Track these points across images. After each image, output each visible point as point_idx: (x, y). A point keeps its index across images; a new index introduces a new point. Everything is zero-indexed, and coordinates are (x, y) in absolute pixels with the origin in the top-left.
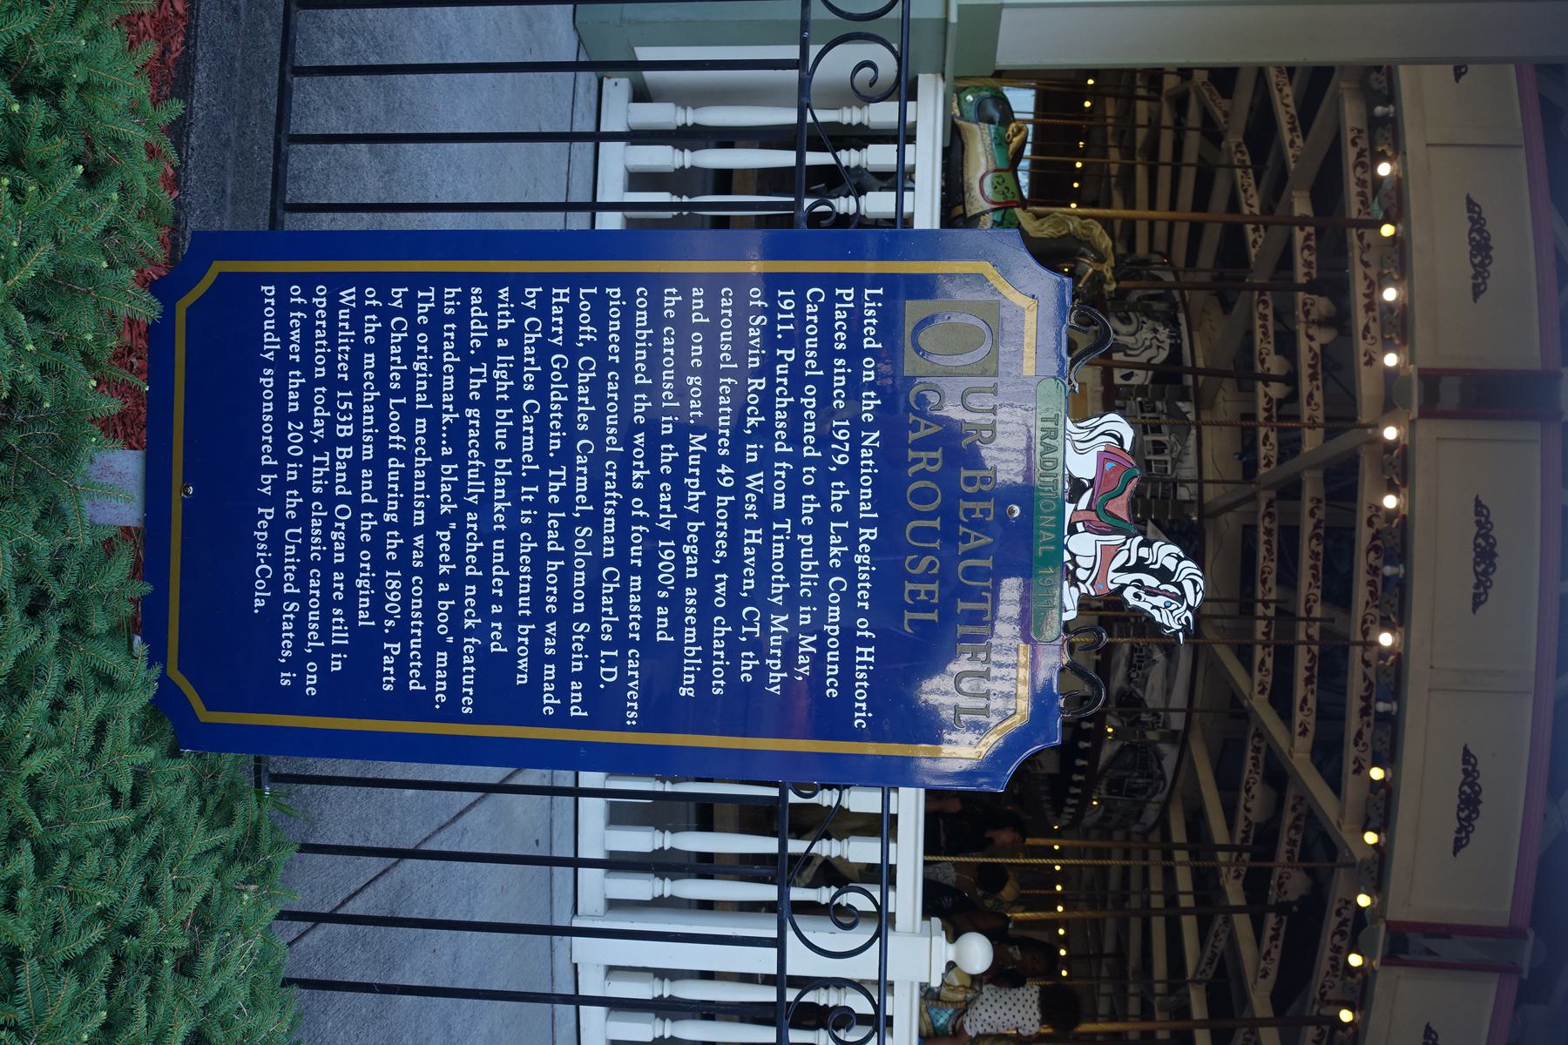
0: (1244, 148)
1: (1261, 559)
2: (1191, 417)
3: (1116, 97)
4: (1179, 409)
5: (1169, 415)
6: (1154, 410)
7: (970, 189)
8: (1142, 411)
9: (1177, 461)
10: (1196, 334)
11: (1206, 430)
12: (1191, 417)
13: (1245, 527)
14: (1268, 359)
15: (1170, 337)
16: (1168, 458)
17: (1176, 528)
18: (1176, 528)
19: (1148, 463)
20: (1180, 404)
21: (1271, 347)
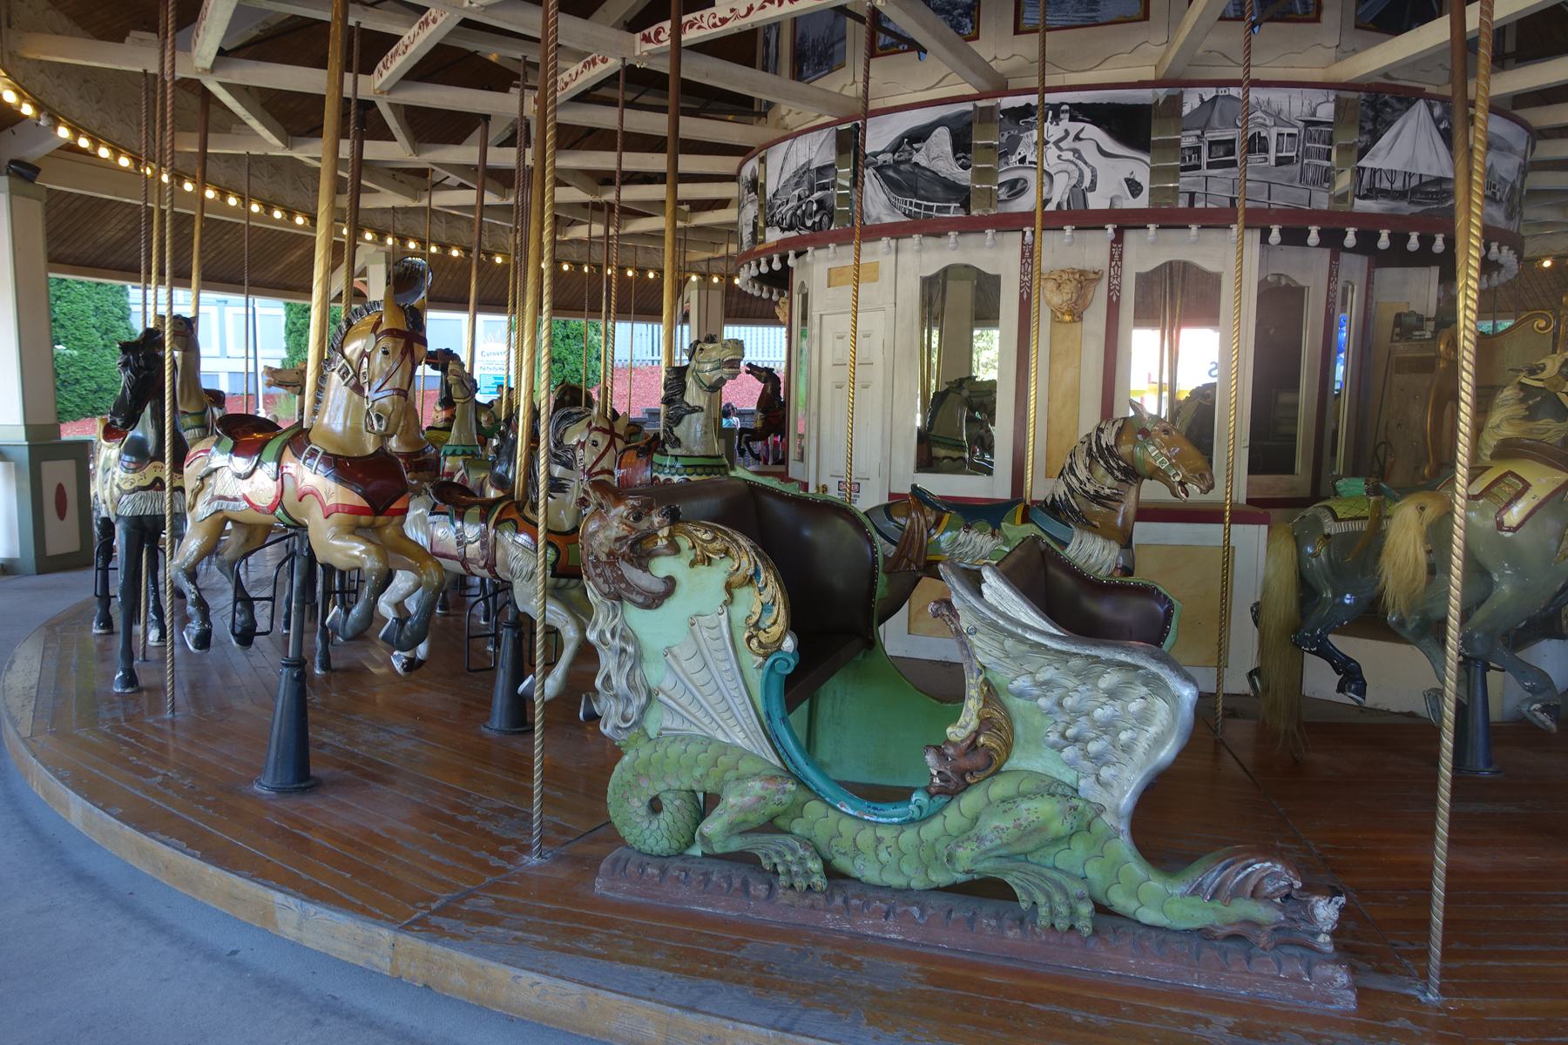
0: (652, 30)
1: (702, 33)
2: (1209, 93)
3: (358, 190)
4: (1194, 113)
5: (1205, 127)
6: (1197, 150)
7: (1096, 645)
8: (1198, 167)
9: (1278, 119)
10: (1013, 85)
11: (1255, 74)
12: (1209, 93)
13: (1357, 27)
14: (720, 15)
15: (1056, 118)
16: (1274, 132)
17: (1369, 126)
18: (1369, 126)
19: (1280, 161)
20: (1186, 110)
21: (707, 12)
